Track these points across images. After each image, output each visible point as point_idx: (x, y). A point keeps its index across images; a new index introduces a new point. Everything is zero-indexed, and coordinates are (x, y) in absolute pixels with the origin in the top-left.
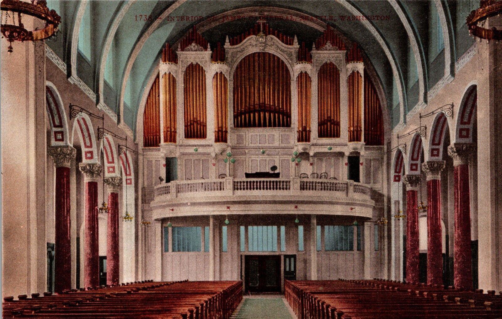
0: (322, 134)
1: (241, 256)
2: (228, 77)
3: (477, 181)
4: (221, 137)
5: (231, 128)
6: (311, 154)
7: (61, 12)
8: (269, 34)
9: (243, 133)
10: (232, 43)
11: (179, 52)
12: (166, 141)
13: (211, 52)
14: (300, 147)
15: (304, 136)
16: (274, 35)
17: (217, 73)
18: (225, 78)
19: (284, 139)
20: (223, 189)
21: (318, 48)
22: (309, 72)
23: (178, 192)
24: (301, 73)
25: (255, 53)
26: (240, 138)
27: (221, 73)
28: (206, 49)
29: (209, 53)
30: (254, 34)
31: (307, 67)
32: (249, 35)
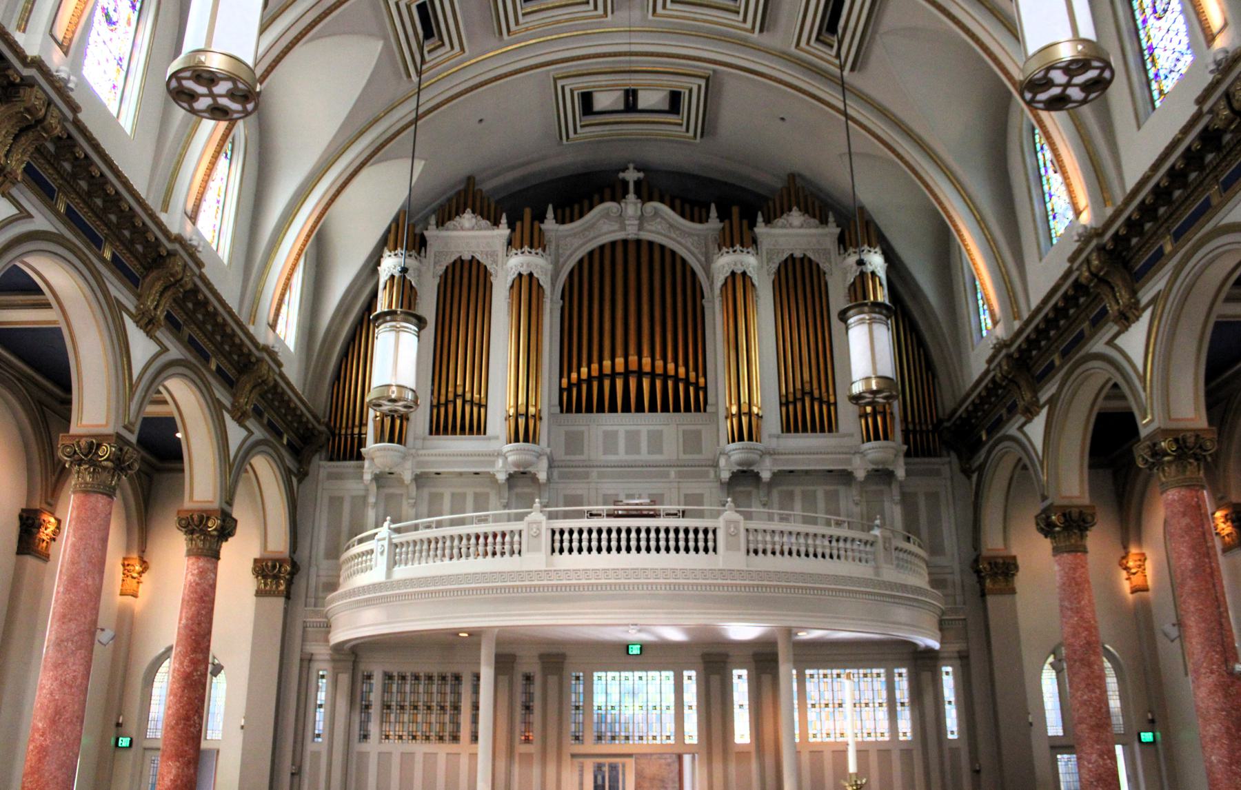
0: (791, 425)
1: (400, 442)
2: (546, 285)
3: (506, 785)
4: (523, 429)
5: (551, 415)
6: (766, 475)
7: (296, 349)
8: (651, 199)
9: (583, 428)
10: (561, 220)
11: (431, 233)
12: (380, 438)
13: (507, 232)
14: (736, 453)
15: (746, 430)
16: (662, 201)
17: (520, 275)
18: (539, 286)
19: (692, 441)
20: (520, 553)
21: (768, 221)
22: (751, 273)
23: (395, 563)
24: (733, 274)
25: (613, 244)
26: (574, 442)
27: (531, 275)
28: (496, 223)
29: (503, 231)
30: (613, 199)
31: (748, 261)
32: (602, 201)
